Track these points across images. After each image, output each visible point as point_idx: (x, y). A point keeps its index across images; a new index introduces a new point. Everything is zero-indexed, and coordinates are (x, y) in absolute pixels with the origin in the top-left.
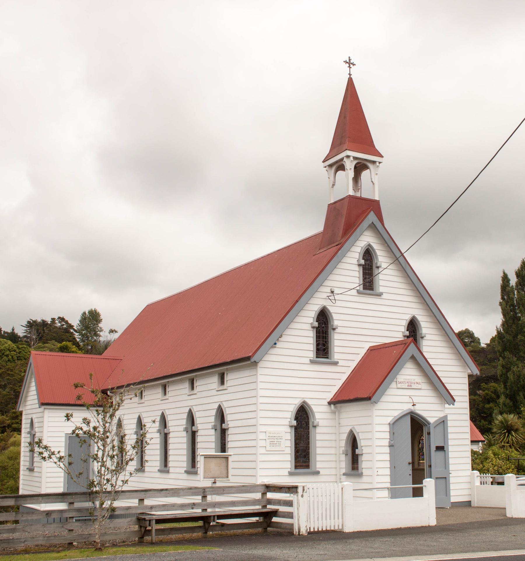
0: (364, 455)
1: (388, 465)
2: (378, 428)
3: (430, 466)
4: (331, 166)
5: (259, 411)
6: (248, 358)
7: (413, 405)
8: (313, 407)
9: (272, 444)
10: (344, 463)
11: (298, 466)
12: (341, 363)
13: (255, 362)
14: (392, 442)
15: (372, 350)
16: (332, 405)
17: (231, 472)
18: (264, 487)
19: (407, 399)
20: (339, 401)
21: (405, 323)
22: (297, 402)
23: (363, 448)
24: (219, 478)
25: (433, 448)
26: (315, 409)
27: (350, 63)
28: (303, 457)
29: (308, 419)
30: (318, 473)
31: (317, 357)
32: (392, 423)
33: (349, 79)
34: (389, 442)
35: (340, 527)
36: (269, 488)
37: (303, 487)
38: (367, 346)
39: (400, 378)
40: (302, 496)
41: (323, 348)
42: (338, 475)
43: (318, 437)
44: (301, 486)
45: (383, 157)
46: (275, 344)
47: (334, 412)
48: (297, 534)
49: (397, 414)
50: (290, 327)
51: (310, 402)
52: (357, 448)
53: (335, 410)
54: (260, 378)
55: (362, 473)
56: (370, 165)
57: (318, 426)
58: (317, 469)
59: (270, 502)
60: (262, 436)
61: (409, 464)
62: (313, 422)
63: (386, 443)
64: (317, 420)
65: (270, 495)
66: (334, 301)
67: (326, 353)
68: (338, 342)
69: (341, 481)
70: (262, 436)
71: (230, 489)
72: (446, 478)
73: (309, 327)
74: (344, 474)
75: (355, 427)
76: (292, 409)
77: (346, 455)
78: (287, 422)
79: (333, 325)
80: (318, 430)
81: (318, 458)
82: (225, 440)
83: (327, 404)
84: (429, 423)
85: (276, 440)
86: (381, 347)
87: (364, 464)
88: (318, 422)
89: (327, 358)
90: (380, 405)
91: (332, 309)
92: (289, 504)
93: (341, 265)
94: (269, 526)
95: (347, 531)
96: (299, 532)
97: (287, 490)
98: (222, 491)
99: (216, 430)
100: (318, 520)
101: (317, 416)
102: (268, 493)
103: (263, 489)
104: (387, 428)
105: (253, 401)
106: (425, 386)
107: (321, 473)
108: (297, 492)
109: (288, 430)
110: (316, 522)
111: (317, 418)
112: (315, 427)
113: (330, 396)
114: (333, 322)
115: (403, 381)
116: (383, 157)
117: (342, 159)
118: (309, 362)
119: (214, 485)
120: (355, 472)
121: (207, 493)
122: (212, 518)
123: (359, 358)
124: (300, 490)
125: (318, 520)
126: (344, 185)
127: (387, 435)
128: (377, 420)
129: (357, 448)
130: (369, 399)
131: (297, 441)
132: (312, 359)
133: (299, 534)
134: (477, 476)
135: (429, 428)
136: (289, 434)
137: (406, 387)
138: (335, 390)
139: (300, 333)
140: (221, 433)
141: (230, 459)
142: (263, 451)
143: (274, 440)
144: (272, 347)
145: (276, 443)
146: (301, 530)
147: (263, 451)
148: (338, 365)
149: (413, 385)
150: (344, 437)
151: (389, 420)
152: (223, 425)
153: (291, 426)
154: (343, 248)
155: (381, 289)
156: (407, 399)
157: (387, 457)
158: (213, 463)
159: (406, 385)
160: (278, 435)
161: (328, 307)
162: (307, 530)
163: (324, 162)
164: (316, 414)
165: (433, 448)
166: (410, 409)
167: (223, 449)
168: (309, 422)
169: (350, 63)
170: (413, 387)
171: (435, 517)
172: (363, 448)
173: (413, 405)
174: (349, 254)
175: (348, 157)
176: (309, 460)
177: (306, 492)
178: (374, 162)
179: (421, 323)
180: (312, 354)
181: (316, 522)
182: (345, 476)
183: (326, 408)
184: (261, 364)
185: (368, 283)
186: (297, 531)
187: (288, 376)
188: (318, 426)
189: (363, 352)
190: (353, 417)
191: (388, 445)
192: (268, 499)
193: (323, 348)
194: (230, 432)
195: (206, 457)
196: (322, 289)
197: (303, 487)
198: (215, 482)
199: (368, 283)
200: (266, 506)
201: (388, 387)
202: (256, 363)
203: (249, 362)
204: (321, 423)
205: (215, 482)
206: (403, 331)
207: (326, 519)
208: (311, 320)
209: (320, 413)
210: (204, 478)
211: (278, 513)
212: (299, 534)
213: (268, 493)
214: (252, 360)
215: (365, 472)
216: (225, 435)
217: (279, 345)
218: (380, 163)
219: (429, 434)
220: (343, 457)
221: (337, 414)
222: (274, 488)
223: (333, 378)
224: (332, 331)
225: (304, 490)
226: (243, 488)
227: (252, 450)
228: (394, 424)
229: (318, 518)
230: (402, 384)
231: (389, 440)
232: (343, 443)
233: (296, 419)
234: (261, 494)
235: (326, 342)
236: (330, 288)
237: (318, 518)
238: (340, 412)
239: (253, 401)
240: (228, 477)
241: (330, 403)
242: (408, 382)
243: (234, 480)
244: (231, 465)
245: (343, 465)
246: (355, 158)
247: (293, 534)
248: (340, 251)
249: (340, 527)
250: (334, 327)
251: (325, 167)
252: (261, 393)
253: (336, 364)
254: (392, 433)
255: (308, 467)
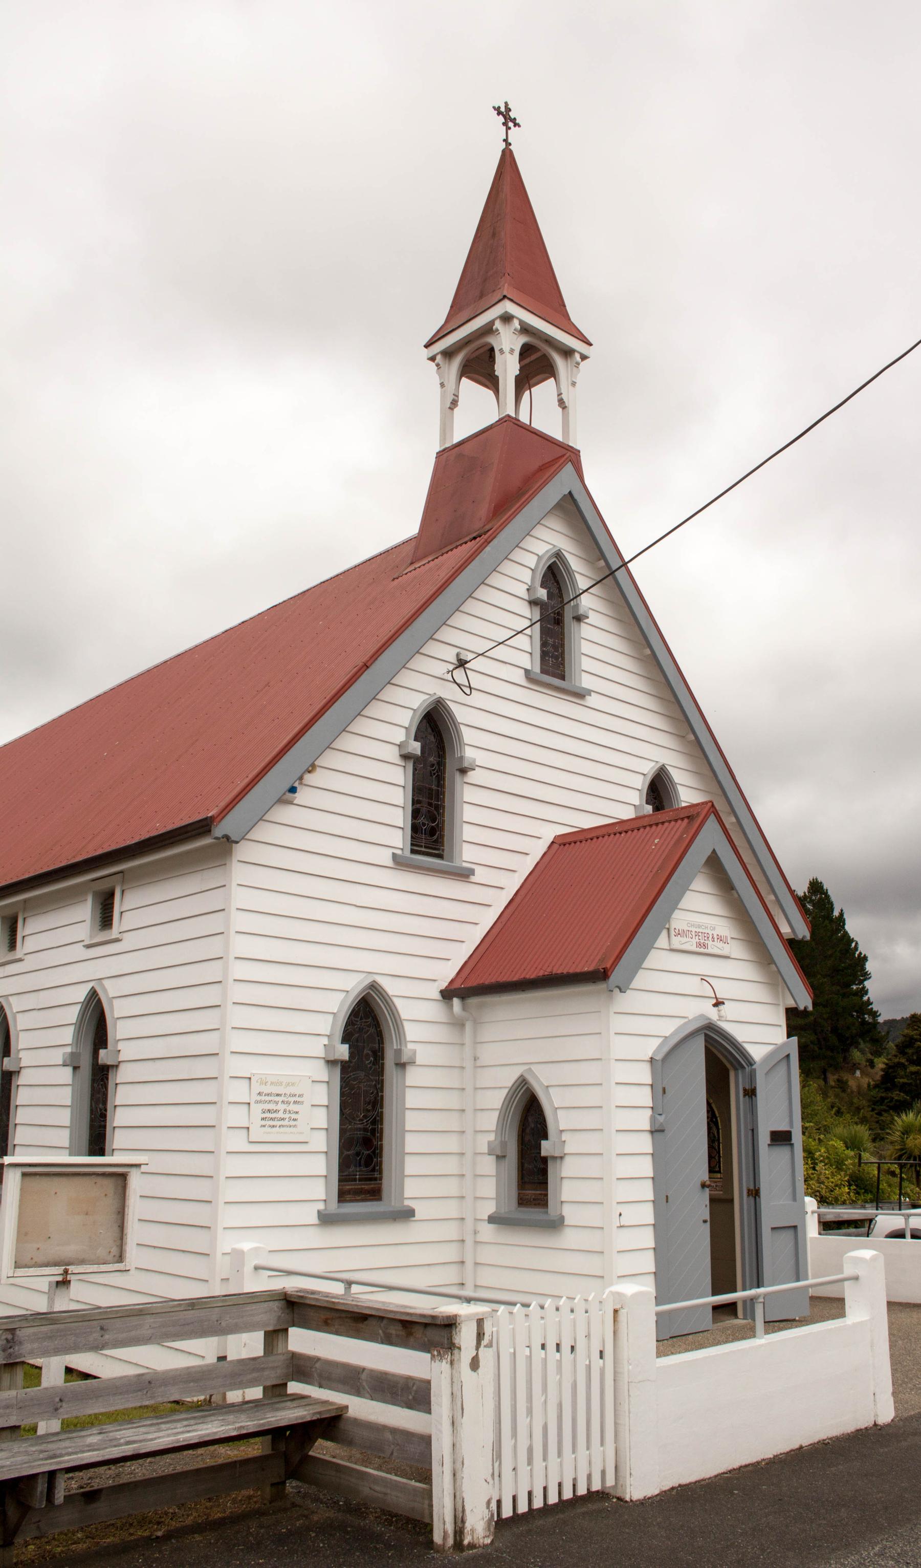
0: (567, 1160)
1: (647, 1191)
2: (621, 1073)
3: (755, 1193)
4: (448, 354)
5: (230, 1005)
6: (203, 827)
7: (716, 1005)
8: (399, 1003)
9: (269, 1117)
10: (490, 1185)
11: (349, 1192)
12: (480, 875)
13: (227, 837)
14: (661, 1119)
15: (562, 843)
16: (456, 1001)
17: (135, 1232)
18: (276, 1305)
19: (692, 985)
20: (476, 986)
21: (641, 783)
22: (352, 986)
23: (564, 1137)
24: (82, 1262)
25: (764, 1139)
26: (405, 1010)
27: (506, 116)
28: (363, 1165)
29: (381, 1041)
30: (407, 1214)
31: (413, 852)
32: (659, 1057)
33: (503, 151)
34: (653, 1120)
35: (610, 1482)
36: (297, 1309)
37: (480, 1322)
38: (549, 833)
39: (680, 920)
40: (475, 1364)
41: (430, 829)
42: (469, 1222)
43: (412, 1099)
44: (469, 1318)
45: (591, 345)
46: (293, 790)
47: (458, 1024)
48: (450, 1541)
49: (669, 1028)
50: (410, 665)
51: (391, 987)
52: (546, 1137)
53: (464, 1014)
54: (240, 898)
55: (562, 1218)
56: (559, 362)
57: (412, 1063)
58: (407, 1203)
59: (302, 1367)
60: (238, 1091)
61: (703, 1186)
62: (399, 1052)
63: (643, 1120)
64: (410, 1046)
65: (301, 1340)
66: (467, 691)
67: (436, 841)
68: (475, 811)
69: (480, 1238)
70: (238, 1091)
71: (135, 1321)
72: (795, 1227)
73: (392, 754)
74: (492, 1219)
75: (533, 1067)
76: (336, 1005)
77: (500, 1158)
78: (317, 1048)
79: (462, 758)
80: (413, 1076)
81: (411, 1166)
82: (105, 1102)
83: (438, 996)
84: (750, 1062)
85: (281, 1107)
86: (599, 833)
87: (569, 1186)
88: (415, 1052)
89: (440, 856)
90: (628, 1001)
91: (461, 714)
92: (416, 1395)
93: (347, 742)
94: (294, 1473)
95: (635, 1498)
96: (459, 1532)
97: (394, 1330)
98: (96, 1335)
99: (75, 1068)
100: (530, 1462)
101: (412, 1032)
102: (293, 1331)
103: (271, 1315)
104: (644, 1075)
105: (211, 972)
106: (736, 949)
107: (418, 1216)
108: (451, 1347)
109: (321, 1072)
110: (524, 1469)
111: (408, 1039)
112: (402, 1066)
113: (447, 973)
114: (462, 749)
115: (686, 928)
116: (591, 345)
117: (489, 329)
118: (390, 863)
119: (62, 1304)
120: (532, 1213)
121: (27, 1347)
122: (41, 1487)
123: (526, 866)
124: (466, 1336)
125: (530, 1462)
126: (478, 409)
127: (645, 1097)
128: (621, 1047)
129: (546, 1137)
130: (600, 976)
131: (347, 1111)
132: (399, 852)
133: (458, 1545)
134: (813, 1212)
135: (752, 1076)
136: (323, 1088)
137: (694, 948)
138: (461, 954)
139: (361, 778)
140: (93, 1081)
141: (136, 1182)
142: (237, 1142)
143: (276, 1108)
144: (282, 801)
145: (281, 1115)
146: (468, 1526)
147: (237, 1142)
148: (473, 879)
149: (710, 943)
150: (496, 1099)
151: (650, 1048)
152: (102, 1052)
153: (331, 1063)
154: (495, 542)
155: (586, 682)
156: (692, 985)
157: (646, 1167)
158: (61, 1199)
159: (695, 940)
160: (288, 1090)
161: (453, 707)
162: (492, 1515)
163: (426, 346)
164: (405, 1024)
165: (764, 1139)
166: (702, 1016)
167: (97, 1141)
168: (382, 1050)
169: (506, 116)
170: (710, 951)
171: (890, 1389)
172: (564, 1137)
173: (716, 1005)
174: (507, 567)
175: (507, 318)
176: (381, 1172)
177: (490, 1345)
178: (567, 353)
179: (680, 788)
180: (399, 839)
181: (524, 1469)
182: (492, 1226)
183: (434, 1010)
184: (243, 851)
185: (554, 659)
186: (450, 1528)
187: (315, 908)
188: (412, 1063)
189: (538, 849)
190: (526, 1040)
191: (648, 1128)
192: (294, 1356)
193: (430, 829)
194: (122, 1075)
195: (31, 1173)
196: (432, 648)
197: (480, 1322)
198: (64, 1283)
199: (554, 659)
200: (285, 1385)
201: (650, 946)
202: (228, 843)
203: (206, 841)
204: (423, 1055)
205: (64, 1283)
206: (637, 803)
207: (560, 1454)
208: (399, 736)
209: (419, 1021)
210: (17, 1265)
211: (342, 1425)
212: (458, 1545)
213: (293, 1331)
214: (219, 831)
215: (570, 1213)
216: (106, 1086)
217: (302, 796)
218: (584, 357)
219: (751, 1093)
220: (488, 1165)
221: (468, 1026)
222: (323, 1315)
223: (458, 918)
224: (458, 775)
225: (480, 1336)
226: (191, 1315)
227: (202, 1140)
228: (660, 1065)
229: (530, 1450)
230: (684, 940)
231: (649, 1112)
232: (490, 1121)
233: (346, 1038)
234: (260, 1336)
235: (437, 808)
236: (458, 650)
237: (530, 1450)
238: (476, 1023)
239: (211, 972)
240: (120, 1258)
241: (447, 994)
242: (697, 934)
243: (148, 1275)
244: (136, 1207)
245: (488, 1188)
246: (525, 329)
247: (430, 1544)
248: (488, 549)
249: (610, 1482)
250: (466, 764)
251: (433, 359)
252: (242, 946)
253: (464, 875)
254: (660, 1090)
255: (375, 1194)
